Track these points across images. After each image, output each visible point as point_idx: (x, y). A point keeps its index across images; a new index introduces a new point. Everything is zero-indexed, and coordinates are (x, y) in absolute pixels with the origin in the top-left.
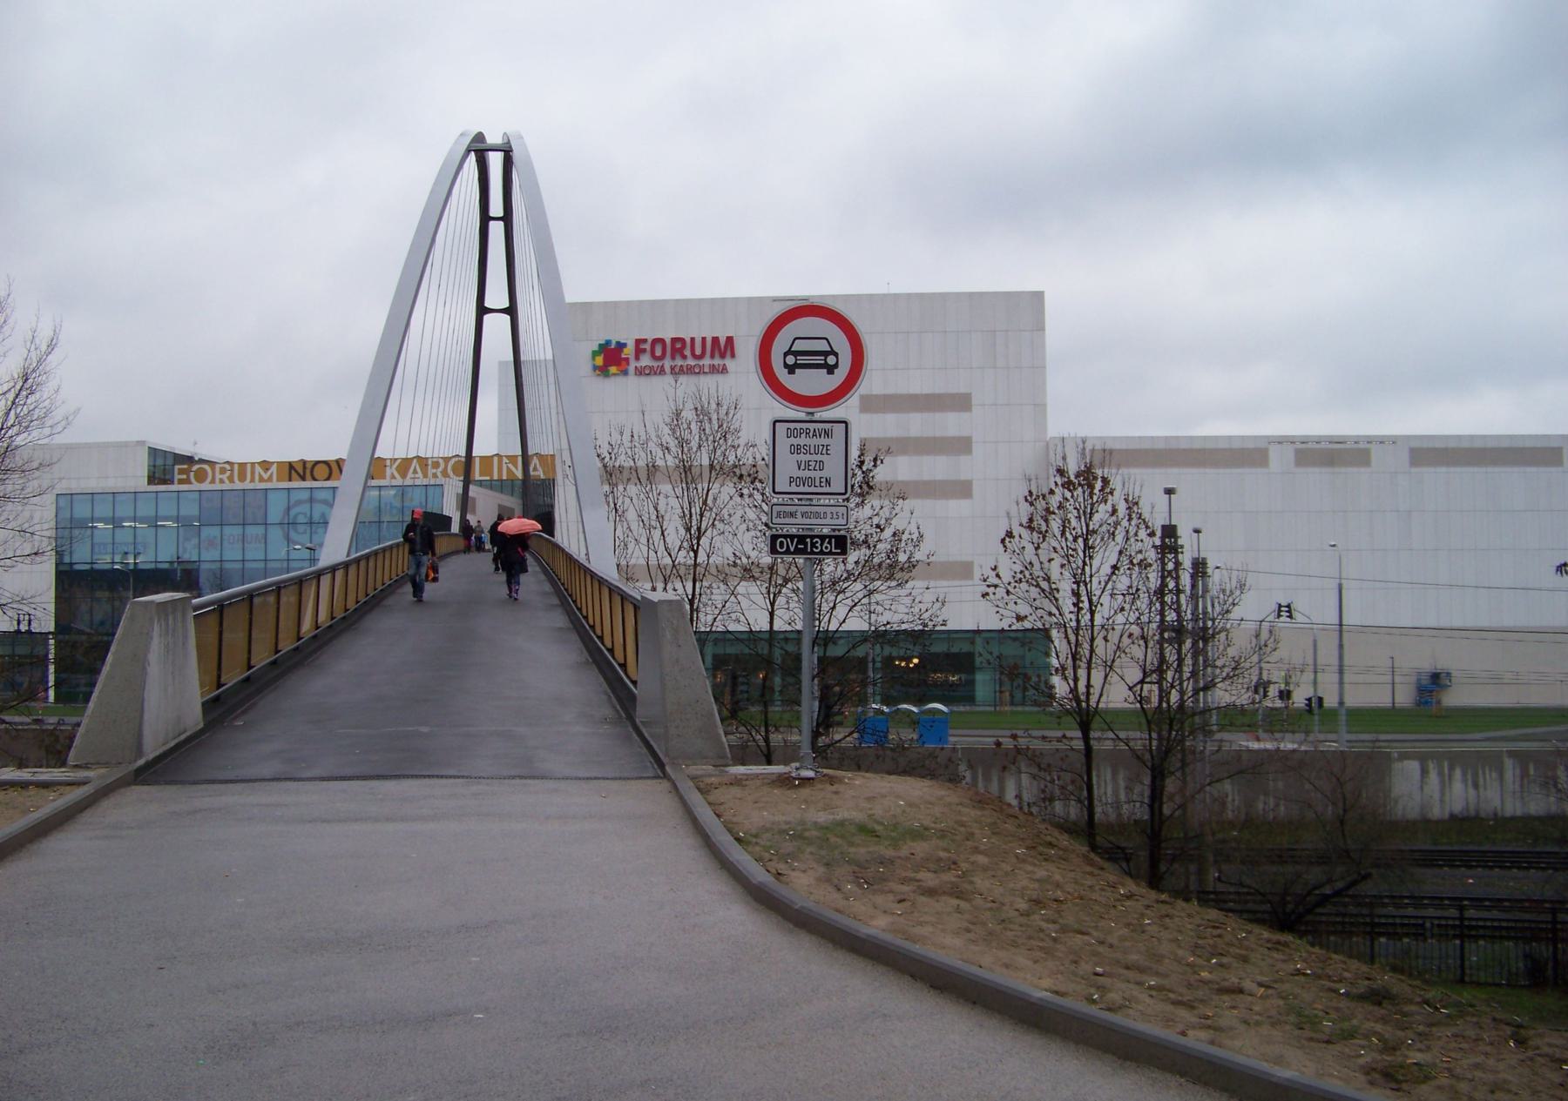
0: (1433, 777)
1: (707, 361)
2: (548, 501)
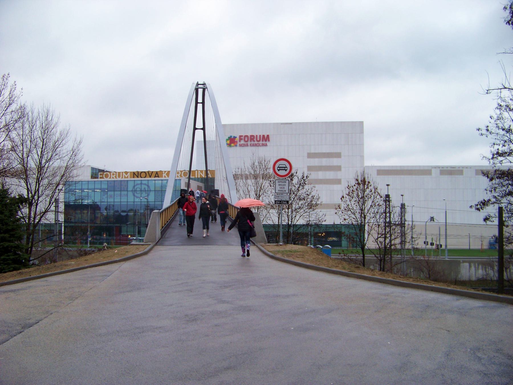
0: (473, 268)
1: (261, 142)
2: (212, 184)
